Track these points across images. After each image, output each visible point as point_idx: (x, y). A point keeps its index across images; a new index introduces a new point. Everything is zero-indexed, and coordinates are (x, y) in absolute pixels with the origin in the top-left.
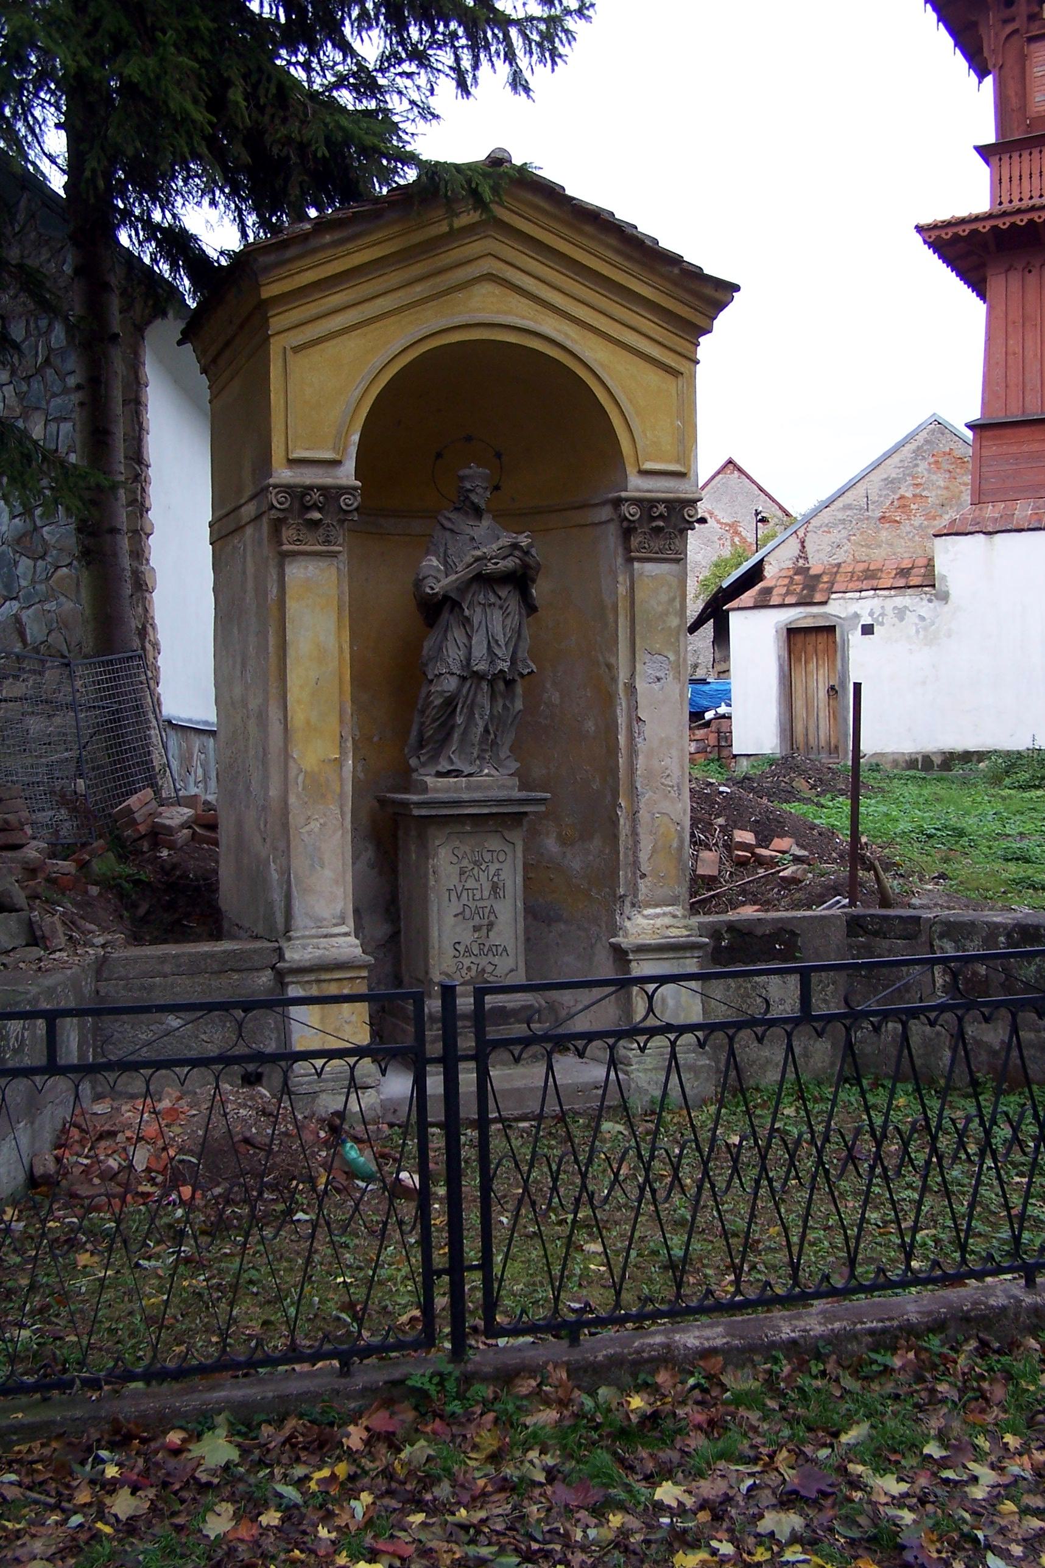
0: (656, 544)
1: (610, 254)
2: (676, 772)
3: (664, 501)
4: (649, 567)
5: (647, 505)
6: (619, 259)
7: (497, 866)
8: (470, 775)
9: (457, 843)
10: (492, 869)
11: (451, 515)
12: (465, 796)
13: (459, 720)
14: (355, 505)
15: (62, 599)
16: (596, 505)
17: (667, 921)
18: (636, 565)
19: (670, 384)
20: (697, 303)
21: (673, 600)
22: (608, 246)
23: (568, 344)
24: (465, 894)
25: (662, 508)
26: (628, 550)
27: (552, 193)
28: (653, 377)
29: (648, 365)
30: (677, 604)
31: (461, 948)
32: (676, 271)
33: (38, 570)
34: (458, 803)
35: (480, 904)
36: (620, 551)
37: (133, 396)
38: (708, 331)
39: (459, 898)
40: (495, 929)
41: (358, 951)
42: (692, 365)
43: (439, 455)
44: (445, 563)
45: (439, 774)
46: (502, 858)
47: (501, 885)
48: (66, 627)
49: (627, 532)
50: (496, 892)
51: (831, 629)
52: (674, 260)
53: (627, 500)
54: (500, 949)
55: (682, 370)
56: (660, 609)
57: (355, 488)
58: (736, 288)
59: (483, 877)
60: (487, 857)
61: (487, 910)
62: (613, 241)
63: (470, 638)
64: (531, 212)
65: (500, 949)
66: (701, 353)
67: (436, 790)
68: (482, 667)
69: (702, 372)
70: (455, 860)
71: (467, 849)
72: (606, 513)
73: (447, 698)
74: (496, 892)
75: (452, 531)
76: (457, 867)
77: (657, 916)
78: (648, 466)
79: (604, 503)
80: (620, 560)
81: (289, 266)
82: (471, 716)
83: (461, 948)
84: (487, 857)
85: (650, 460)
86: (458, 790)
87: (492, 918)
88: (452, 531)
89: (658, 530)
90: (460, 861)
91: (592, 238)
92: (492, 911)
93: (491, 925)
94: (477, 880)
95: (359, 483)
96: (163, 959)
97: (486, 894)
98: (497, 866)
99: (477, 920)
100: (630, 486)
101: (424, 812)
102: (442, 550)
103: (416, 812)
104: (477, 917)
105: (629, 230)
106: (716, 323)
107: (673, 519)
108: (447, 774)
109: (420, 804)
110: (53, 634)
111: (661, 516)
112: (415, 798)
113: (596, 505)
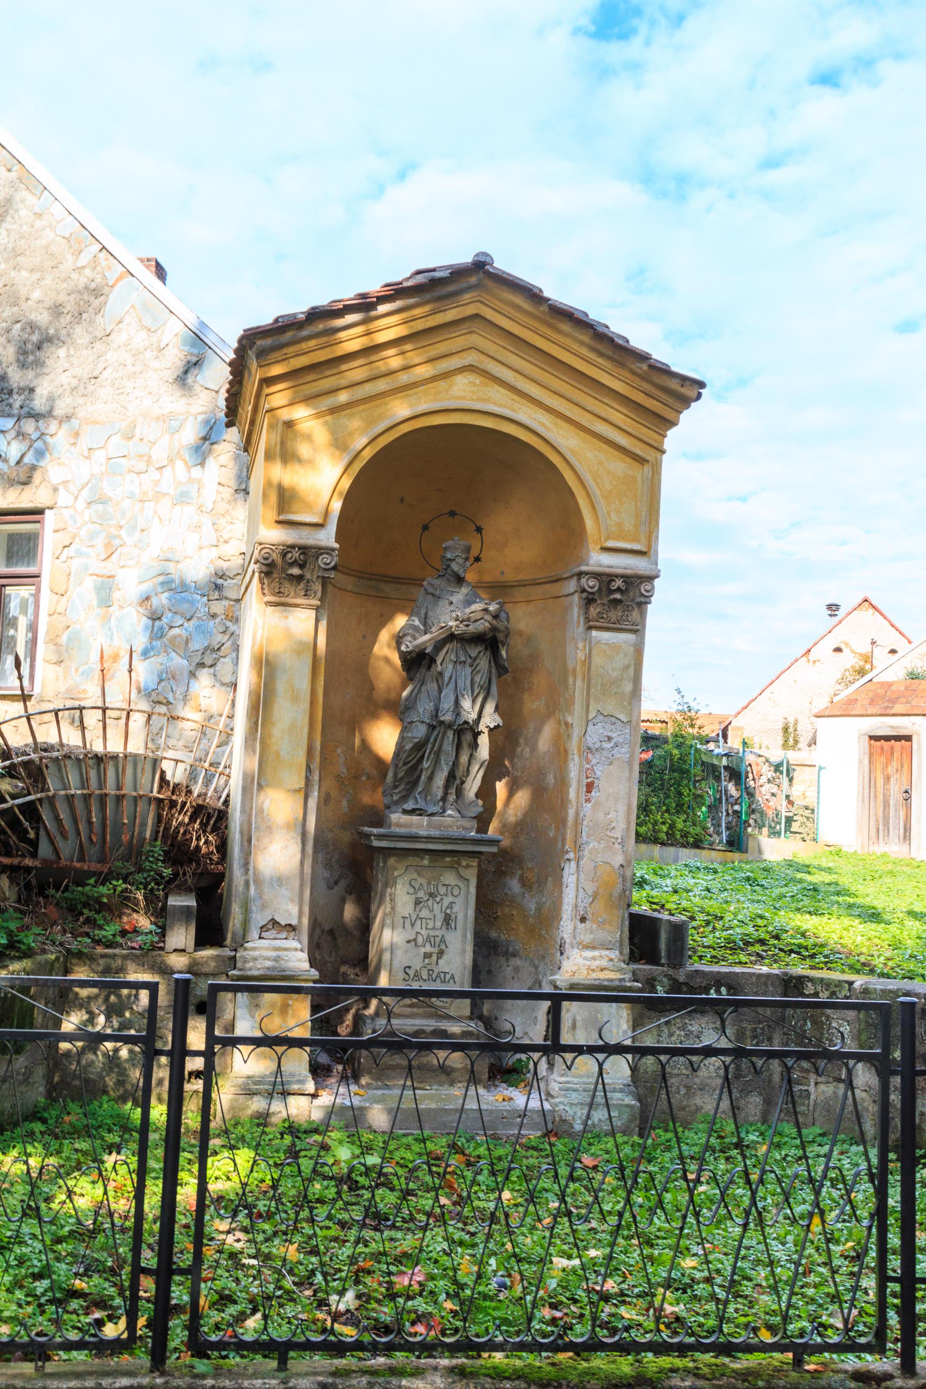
0: (614, 615)
1: (584, 351)
2: (622, 825)
3: (622, 576)
4: (605, 636)
5: (605, 579)
6: (592, 356)
7: (451, 899)
8: (432, 815)
9: (415, 875)
10: (446, 902)
11: (434, 582)
12: (423, 833)
13: (425, 764)
14: (333, 564)
15: (173, 654)
16: (566, 578)
17: (604, 963)
18: (594, 633)
19: (641, 473)
20: (664, 397)
21: (627, 667)
22: (582, 343)
23: (541, 430)
24: (419, 922)
25: (619, 583)
26: (587, 620)
27: (533, 295)
28: (620, 466)
29: (616, 453)
30: (631, 672)
31: (411, 972)
32: (645, 367)
33: (156, 629)
34: (415, 838)
35: (432, 933)
36: (582, 620)
37: (243, 487)
38: (673, 424)
39: (413, 925)
40: (445, 957)
41: (306, 965)
42: (658, 454)
43: (426, 528)
44: (425, 624)
45: (405, 812)
46: (456, 892)
47: (453, 916)
48: (174, 678)
49: (589, 601)
50: (448, 924)
51: (908, 738)
52: (643, 357)
53: (586, 573)
54: (448, 977)
55: (648, 458)
56: (615, 674)
57: (333, 550)
58: (702, 385)
59: (437, 908)
60: (442, 890)
61: (438, 940)
62: (585, 338)
63: (440, 691)
64: (510, 310)
65: (448, 977)
66: (668, 444)
67: (399, 825)
68: (448, 717)
69: (667, 461)
70: (412, 891)
71: (424, 882)
72: (572, 586)
73: (416, 744)
74: (448, 924)
75: (433, 595)
76: (414, 897)
77: (594, 958)
78: (610, 544)
79: (572, 577)
80: (581, 628)
81: (285, 351)
82: (437, 762)
83: (411, 972)
84: (442, 890)
85: (614, 539)
86: (420, 826)
87: (443, 947)
88: (433, 595)
89: (616, 602)
90: (416, 892)
91: (567, 335)
92: (443, 940)
93: (441, 953)
94: (431, 911)
95: (337, 546)
96: (871, 1048)
97: (438, 924)
98: (451, 899)
99: (428, 949)
100: (592, 561)
101: (384, 844)
102: (423, 611)
103: (376, 843)
104: (428, 945)
105: (601, 329)
106: (682, 416)
107: (631, 594)
108: (412, 812)
109: (380, 837)
110: (163, 684)
111: (619, 590)
112: (375, 831)
113: (566, 578)
